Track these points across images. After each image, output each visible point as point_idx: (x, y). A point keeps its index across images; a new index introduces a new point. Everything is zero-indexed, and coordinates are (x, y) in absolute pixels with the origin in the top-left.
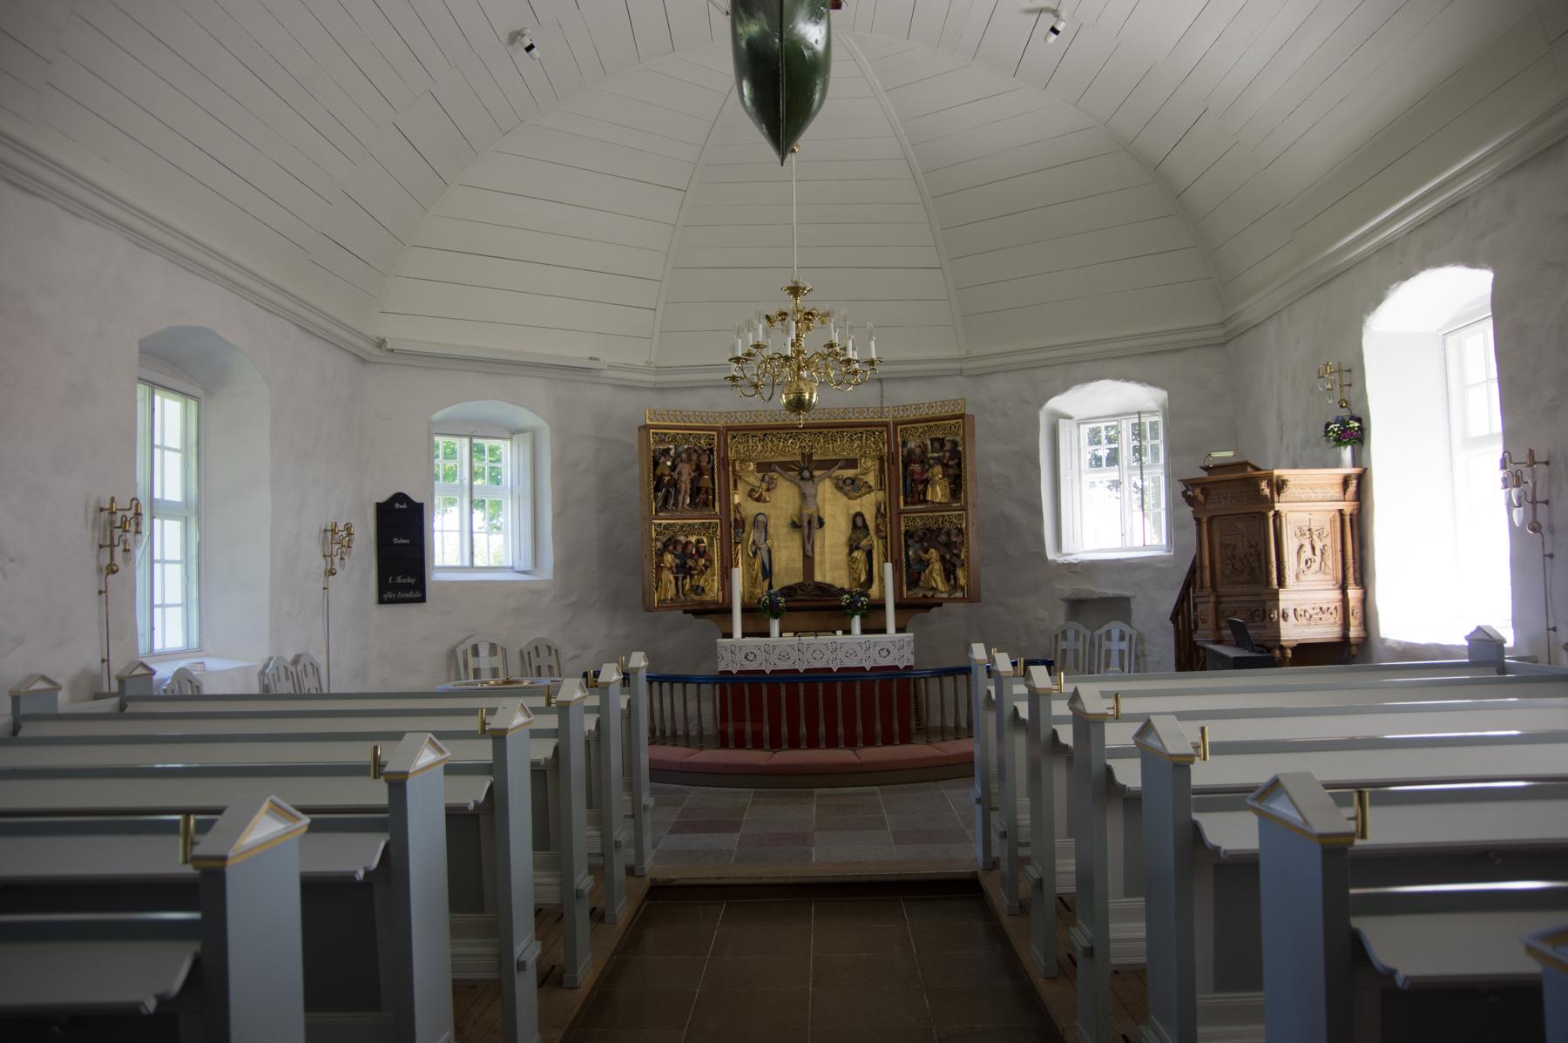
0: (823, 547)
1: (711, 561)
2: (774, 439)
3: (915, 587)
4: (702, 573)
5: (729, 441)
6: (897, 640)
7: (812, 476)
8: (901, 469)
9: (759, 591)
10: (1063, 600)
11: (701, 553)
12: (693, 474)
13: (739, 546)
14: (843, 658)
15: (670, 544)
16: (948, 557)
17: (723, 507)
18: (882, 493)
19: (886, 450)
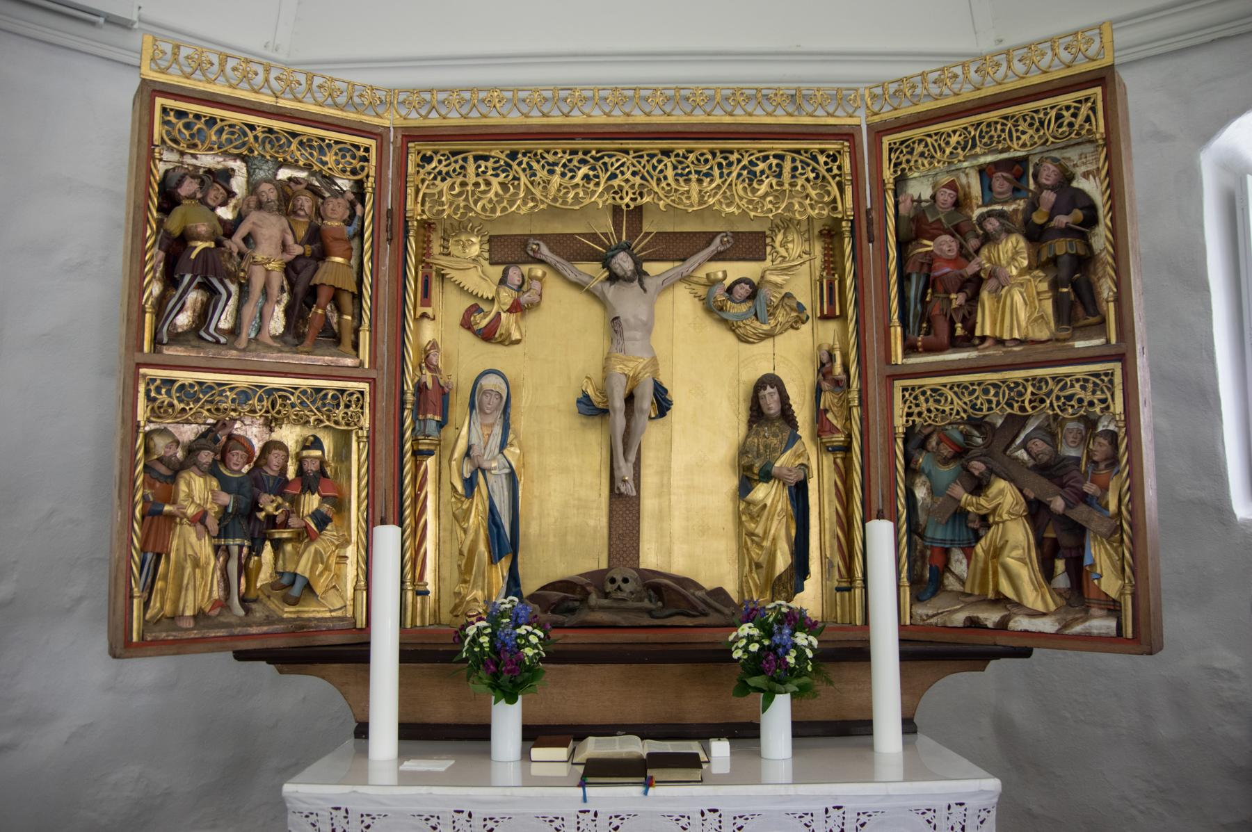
0: (665, 470)
2: (535, 165)
3: (934, 594)
4: (304, 536)
5: (411, 169)
6: (941, 804)
7: (640, 274)
8: (893, 253)
9: (479, 594)
12: (298, 250)
13: (430, 462)
16: (1058, 504)
17: (383, 348)
18: (832, 327)
19: (849, 203)
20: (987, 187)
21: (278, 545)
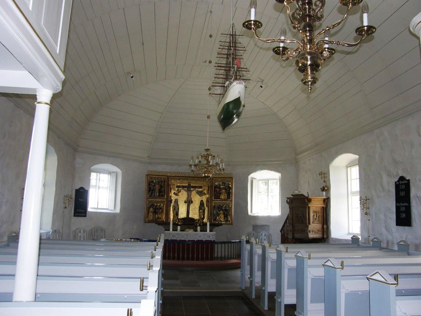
1: (163, 211)
10: (252, 225)
11: (161, 208)
14: (198, 238)
15: (153, 205)
16: (226, 213)
18: (208, 195)
20: (222, 184)
21: (158, 214)
